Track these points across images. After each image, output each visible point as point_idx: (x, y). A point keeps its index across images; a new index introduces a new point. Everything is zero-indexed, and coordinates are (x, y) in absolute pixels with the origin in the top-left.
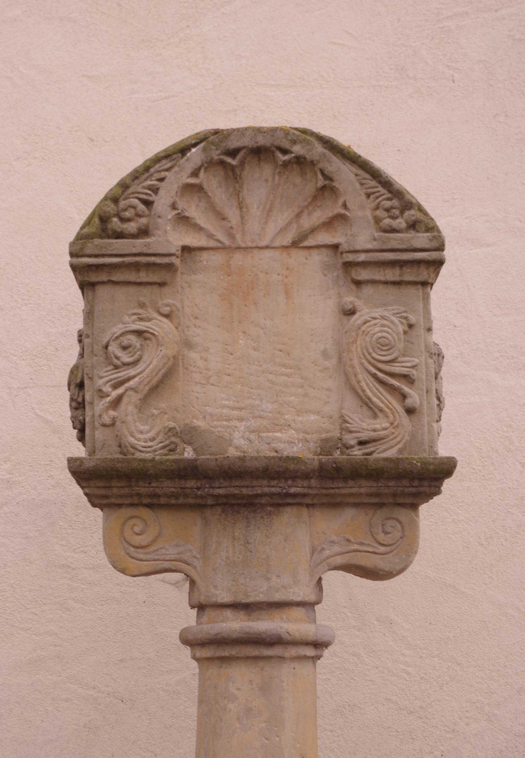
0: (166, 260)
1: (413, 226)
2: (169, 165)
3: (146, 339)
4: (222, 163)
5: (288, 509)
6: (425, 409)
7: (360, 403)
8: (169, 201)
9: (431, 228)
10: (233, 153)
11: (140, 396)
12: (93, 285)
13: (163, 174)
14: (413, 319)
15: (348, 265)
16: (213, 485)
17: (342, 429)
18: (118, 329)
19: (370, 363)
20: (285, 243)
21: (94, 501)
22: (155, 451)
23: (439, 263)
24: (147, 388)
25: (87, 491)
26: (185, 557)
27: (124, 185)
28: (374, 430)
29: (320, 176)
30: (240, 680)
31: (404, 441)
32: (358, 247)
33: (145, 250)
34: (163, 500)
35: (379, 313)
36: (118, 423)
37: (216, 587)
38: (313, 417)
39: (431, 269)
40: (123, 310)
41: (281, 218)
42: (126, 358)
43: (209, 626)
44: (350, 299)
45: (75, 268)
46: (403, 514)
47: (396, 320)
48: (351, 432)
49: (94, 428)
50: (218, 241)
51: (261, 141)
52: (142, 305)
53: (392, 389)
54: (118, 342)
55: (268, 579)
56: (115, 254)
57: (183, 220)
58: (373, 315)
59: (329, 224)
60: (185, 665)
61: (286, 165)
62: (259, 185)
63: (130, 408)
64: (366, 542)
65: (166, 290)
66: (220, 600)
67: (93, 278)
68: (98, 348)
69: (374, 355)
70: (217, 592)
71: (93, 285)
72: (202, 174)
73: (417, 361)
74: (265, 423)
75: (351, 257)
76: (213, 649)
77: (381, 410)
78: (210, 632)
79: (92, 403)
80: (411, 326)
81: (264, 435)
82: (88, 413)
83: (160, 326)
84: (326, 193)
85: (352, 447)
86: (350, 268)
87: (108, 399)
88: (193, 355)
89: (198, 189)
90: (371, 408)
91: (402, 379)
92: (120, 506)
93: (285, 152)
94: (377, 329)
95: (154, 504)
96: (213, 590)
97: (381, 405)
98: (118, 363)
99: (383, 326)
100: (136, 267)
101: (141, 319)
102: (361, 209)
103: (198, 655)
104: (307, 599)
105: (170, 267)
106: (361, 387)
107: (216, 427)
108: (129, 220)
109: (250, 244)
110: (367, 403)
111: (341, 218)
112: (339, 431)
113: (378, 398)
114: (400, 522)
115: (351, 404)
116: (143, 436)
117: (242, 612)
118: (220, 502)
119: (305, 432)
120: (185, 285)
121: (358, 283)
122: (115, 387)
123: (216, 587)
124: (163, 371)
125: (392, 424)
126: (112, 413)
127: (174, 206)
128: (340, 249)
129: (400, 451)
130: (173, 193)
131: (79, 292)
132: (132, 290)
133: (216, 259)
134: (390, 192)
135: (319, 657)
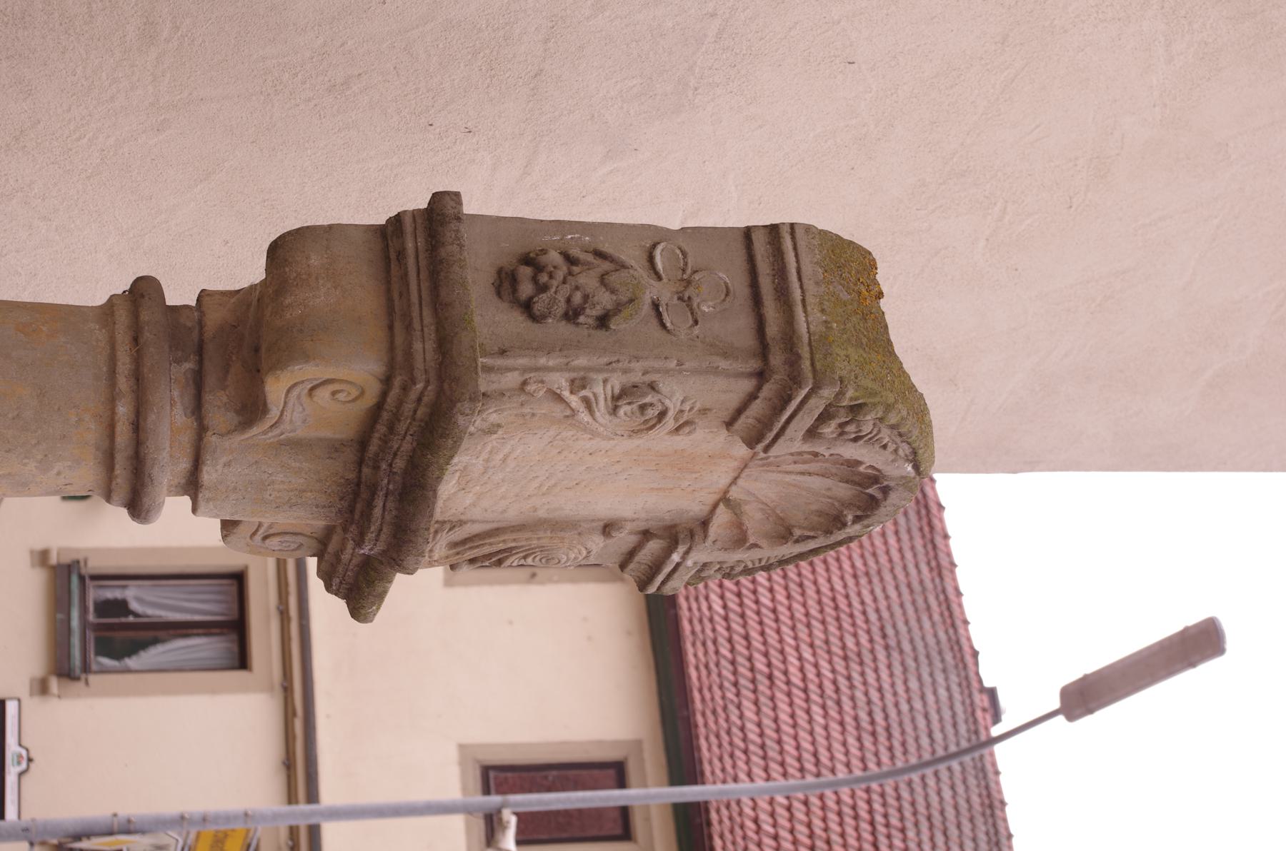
16: (391, 498)
37: (227, 465)
70: (219, 467)
78: (156, 468)
112: (441, 519)
123: (227, 465)
131: (768, 223)
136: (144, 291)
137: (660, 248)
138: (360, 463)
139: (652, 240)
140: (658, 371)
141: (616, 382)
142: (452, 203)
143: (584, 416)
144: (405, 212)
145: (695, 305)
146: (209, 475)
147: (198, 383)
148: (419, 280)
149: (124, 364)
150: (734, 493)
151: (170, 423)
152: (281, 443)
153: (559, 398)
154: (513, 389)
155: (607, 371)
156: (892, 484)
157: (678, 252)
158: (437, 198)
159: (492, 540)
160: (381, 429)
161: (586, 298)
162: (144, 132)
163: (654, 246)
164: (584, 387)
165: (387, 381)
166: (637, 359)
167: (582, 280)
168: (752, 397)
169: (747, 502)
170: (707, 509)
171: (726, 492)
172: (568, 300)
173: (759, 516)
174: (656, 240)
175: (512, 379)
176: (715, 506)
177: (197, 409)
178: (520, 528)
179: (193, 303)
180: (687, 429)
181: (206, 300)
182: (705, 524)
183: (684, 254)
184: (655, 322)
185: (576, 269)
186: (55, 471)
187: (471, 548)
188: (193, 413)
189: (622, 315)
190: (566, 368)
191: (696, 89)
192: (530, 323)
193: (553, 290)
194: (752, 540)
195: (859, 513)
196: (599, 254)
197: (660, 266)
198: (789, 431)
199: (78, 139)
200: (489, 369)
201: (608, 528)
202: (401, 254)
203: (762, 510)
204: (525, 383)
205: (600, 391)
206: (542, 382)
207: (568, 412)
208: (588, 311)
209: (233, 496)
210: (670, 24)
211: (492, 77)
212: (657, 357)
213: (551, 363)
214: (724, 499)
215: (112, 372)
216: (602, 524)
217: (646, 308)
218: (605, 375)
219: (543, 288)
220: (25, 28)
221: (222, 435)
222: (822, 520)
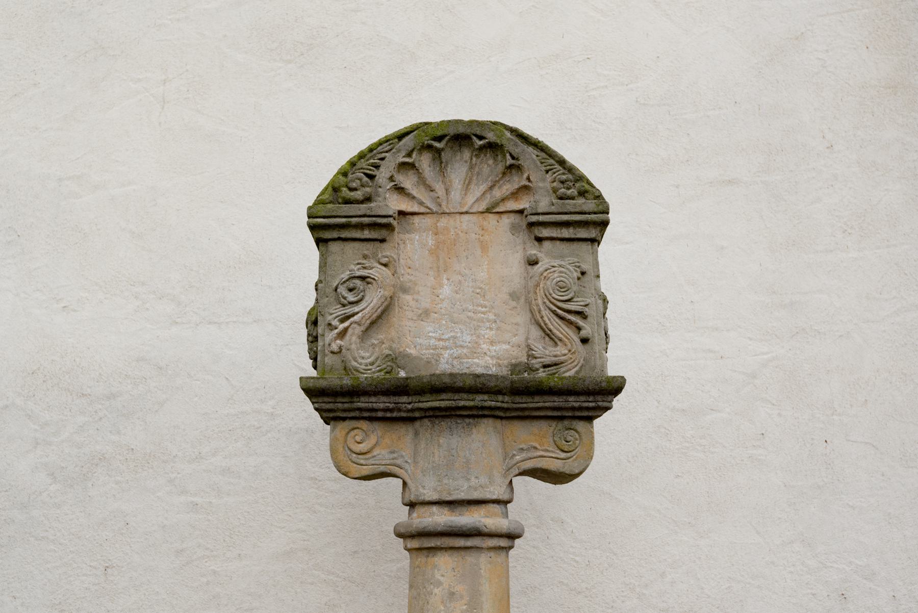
0: (384, 221)
1: (582, 193)
2: (389, 148)
3: (368, 283)
4: (429, 147)
5: (485, 421)
6: (596, 340)
7: (543, 335)
8: (388, 175)
9: (599, 197)
10: (439, 139)
11: (363, 328)
12: (326, 241)
13: (383, 155)
14: (585, 267)
15: (531, 225)
17: (529, 356)
18: (345, 276)
19: (551, 302)
20: (480, 210)
21: (329, 417)
22: (374, 373)
23: (604, 224)
24: (368, 322)
25: (316, 405)
26: (399, 462)
27: (352, 164)
28: (555, 356)
29: (508, 157)
30: (445, 567)
31: (580, 365)
32: (540, 211)
33: (369, 213)
34: (380, 414)
35: (556, 262)
36: (343, 351)
37: (423, 487)
38: (505, 347)
39: (599, 229)
40: (349, 258)
41: (477, 190)
42: (351, 297)
43: (419, 520)
44: (533, 251)
45: (313, 228)
46: (581, 426)
47: (571, 268)
48: (536, 358)
49: (325, 355)
50: (427, 207)
51: (461, 130)
52: (365, 257)
53: (570, 323)
54: (345, 285)
55: (469, 480)
56: (348, 218)
57: (399, 189)
58: (553, 264)
59: (515, 195)
60: (398, 555)
61: (481, 148)
62: (459, 167)
63: (354, 338)
64: (551, 449)
65: (384, 245)
66: (427, 499)
67: (327, 235)
68: (329, 290)
69: (554, 295)
70: (425, 492)
71: (326, 241)
72: (414, 155)
73: (588, 301)
74: (465, 351)
75: (534, 219)
76: (423, 541)
77: (561, 340)
79: (323, 335)
80: (583, 273)
81: (465, 360)
82: (320, 343)
83: (377, 271)
84: (513, 171)
85: (538, 370)
86: (535, 227)
87: (336, 331)
88: (407, 298)
89: (412, 166)
90: (551, 338)
91: (577, 314)
92: (344, 419)
93: (481, 138)
94: (556, 275)
95: (372, 417)
96: (421, 490)
97: (561, 336)
98: (346, 302)
99: (561, 272)
100: (361, 227)
101: (365, 268)
102: (543, 183)
103: (409, 546)
104: (501, 497)
105: (389, 227)
106: (544, 321)
107: (425, 354)
108: (355, 189)
109: (452, 210)
110: (548, 334)
111: (525, 188)
113: (558, 330)
114: (576, 431)
115: (535, 333)
116: (365, 360)
117: (446, 509)
118: (427, 414)
119: (498, 358)
120: (400, 242)
121: (539, 240)
122: (342, 321)
123: (423, 487)
124: (381, 308)
125: (570, 351)
126: (338, 342)
127: (391, 179)
128: (525, 213)
129: (577, 372)
130: (391, 169)
132: (357, 245)
133: (428, 221)
134: (564, 168)
135: (511, 547)
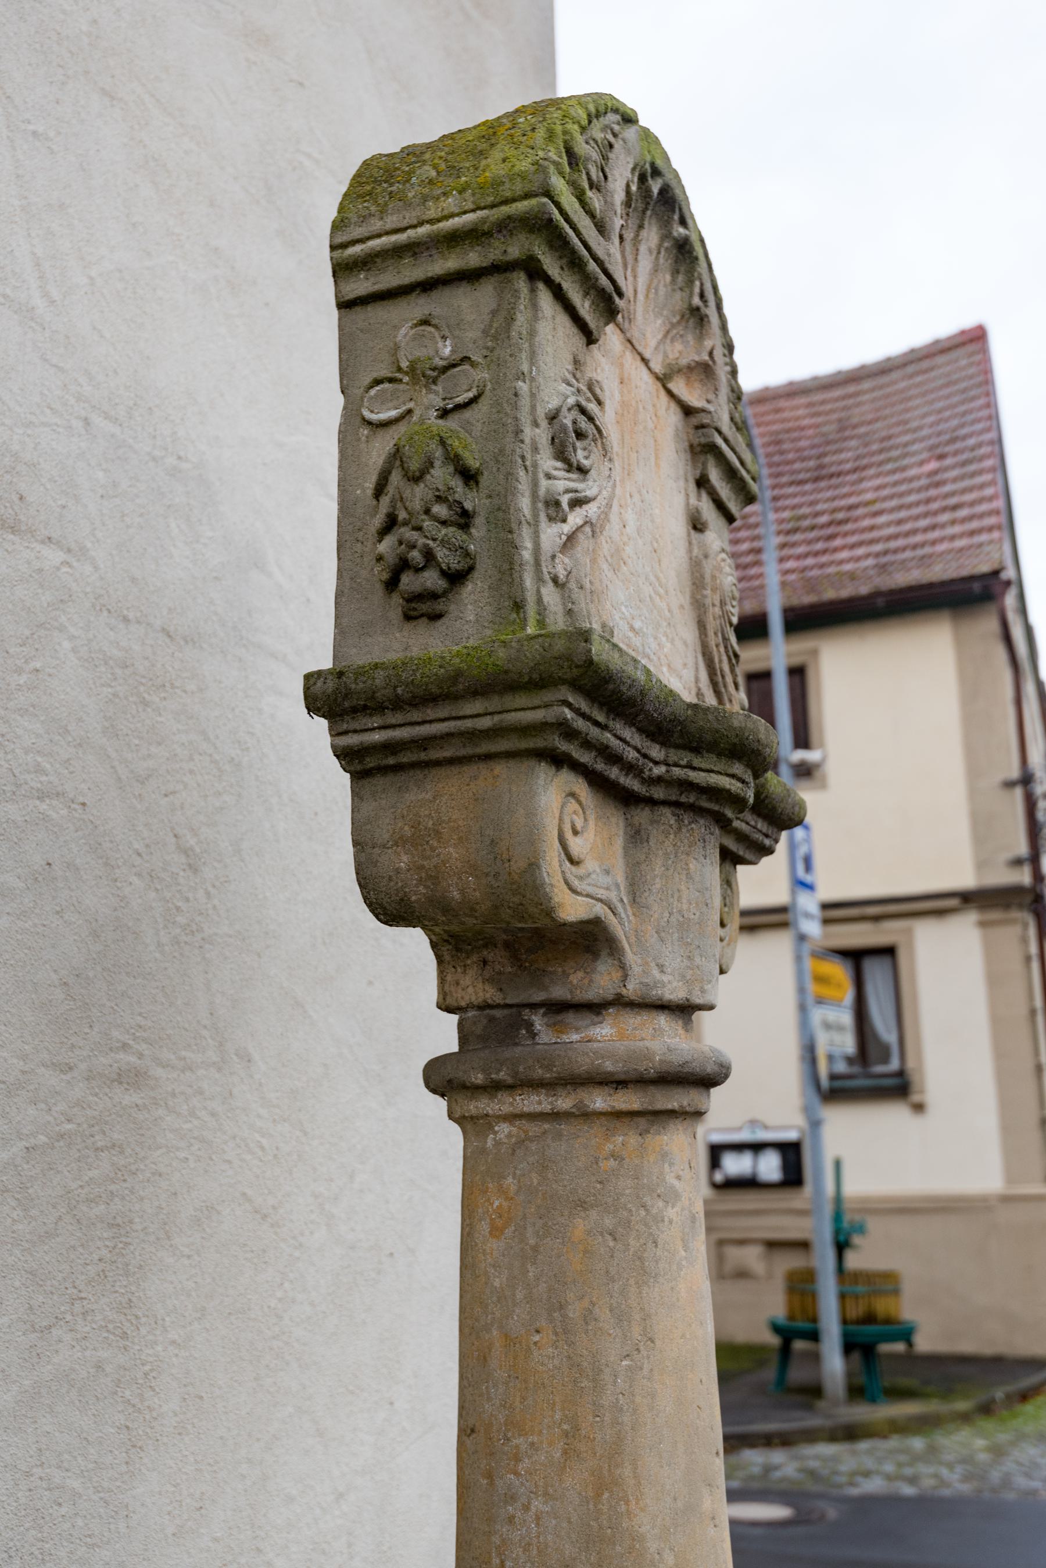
37: (661, 968)
70: (665, 978)
123: (661, 968)
136: (440, 1078)
137: (367, 414)
138: (652, 802)
139: (355, 426)
140: (533, 408)
141: (548, 463)
142: (319, 684)
143: (591, 510)
144: (332, 746)
145: (442, 363)
146: (674, 991)
147: (559, 1009)
148: (424, 722)
149: (540, 1103)
150: (657, 366)
151: (607, 1039)
152: (634, 901)
153: (571, 538)
154: (563, 597)
155: (535, 474)
156: (648, 158)
157: (373, 392)
158: (314, 704)
159: (716, 660)
160: (614, 773)
161: (439, 499)
162: (251, 1077)
163: (370, 423)
164: (557, 504)
165: (559, 761)
166: (518, 432)
167: (417, 505)
168: (559, 294)
169: (666, 356)
170: (673, 406)
171: (658, 378)
172: (444, 523)
173: (678, 346)
174: (359, 419)
175: (550, 595)
176: (670, 393)
177: (595, 1008)
178: (701, 626)
179: (454, 1018)
180: (598, 391)
181: (451, 1001)
182: (688, 411)
183: (378, 382)
184: (467, 414)
185: (402, 515)
186: (676, 1182)
187: (725, 686)
188: (599, 1014)
189: (460, 451)
190: (535, 525)
191: (179, 458)
192: (476, 574)
193: (430, 542)
194: (706, 357)
195: (676, 217)
196: (379, 491)
197: (393, 413)
198: (600, 253)
199: (262, 1148)
200: (541, 623)
201: (697, 525)
202: (389, 748)
203: (672, 341)
204: (555, 580)
205: (563, 483)
206: (553, 557)
207: (588, 529)
208: (457, 497)
209: (698, 960)
210: (100, 475)
211: (173, 686)
212: (516, 407)
213: (529, 545)
214: (663, 380)
215: (555, 1116)
216: (692, 532)
217: (452, 423)
218: (541, 475)
219: (429, 555)
220: (131, 1222)
221: (625, 977)
222: (682, 269)
